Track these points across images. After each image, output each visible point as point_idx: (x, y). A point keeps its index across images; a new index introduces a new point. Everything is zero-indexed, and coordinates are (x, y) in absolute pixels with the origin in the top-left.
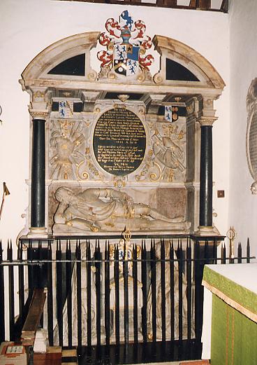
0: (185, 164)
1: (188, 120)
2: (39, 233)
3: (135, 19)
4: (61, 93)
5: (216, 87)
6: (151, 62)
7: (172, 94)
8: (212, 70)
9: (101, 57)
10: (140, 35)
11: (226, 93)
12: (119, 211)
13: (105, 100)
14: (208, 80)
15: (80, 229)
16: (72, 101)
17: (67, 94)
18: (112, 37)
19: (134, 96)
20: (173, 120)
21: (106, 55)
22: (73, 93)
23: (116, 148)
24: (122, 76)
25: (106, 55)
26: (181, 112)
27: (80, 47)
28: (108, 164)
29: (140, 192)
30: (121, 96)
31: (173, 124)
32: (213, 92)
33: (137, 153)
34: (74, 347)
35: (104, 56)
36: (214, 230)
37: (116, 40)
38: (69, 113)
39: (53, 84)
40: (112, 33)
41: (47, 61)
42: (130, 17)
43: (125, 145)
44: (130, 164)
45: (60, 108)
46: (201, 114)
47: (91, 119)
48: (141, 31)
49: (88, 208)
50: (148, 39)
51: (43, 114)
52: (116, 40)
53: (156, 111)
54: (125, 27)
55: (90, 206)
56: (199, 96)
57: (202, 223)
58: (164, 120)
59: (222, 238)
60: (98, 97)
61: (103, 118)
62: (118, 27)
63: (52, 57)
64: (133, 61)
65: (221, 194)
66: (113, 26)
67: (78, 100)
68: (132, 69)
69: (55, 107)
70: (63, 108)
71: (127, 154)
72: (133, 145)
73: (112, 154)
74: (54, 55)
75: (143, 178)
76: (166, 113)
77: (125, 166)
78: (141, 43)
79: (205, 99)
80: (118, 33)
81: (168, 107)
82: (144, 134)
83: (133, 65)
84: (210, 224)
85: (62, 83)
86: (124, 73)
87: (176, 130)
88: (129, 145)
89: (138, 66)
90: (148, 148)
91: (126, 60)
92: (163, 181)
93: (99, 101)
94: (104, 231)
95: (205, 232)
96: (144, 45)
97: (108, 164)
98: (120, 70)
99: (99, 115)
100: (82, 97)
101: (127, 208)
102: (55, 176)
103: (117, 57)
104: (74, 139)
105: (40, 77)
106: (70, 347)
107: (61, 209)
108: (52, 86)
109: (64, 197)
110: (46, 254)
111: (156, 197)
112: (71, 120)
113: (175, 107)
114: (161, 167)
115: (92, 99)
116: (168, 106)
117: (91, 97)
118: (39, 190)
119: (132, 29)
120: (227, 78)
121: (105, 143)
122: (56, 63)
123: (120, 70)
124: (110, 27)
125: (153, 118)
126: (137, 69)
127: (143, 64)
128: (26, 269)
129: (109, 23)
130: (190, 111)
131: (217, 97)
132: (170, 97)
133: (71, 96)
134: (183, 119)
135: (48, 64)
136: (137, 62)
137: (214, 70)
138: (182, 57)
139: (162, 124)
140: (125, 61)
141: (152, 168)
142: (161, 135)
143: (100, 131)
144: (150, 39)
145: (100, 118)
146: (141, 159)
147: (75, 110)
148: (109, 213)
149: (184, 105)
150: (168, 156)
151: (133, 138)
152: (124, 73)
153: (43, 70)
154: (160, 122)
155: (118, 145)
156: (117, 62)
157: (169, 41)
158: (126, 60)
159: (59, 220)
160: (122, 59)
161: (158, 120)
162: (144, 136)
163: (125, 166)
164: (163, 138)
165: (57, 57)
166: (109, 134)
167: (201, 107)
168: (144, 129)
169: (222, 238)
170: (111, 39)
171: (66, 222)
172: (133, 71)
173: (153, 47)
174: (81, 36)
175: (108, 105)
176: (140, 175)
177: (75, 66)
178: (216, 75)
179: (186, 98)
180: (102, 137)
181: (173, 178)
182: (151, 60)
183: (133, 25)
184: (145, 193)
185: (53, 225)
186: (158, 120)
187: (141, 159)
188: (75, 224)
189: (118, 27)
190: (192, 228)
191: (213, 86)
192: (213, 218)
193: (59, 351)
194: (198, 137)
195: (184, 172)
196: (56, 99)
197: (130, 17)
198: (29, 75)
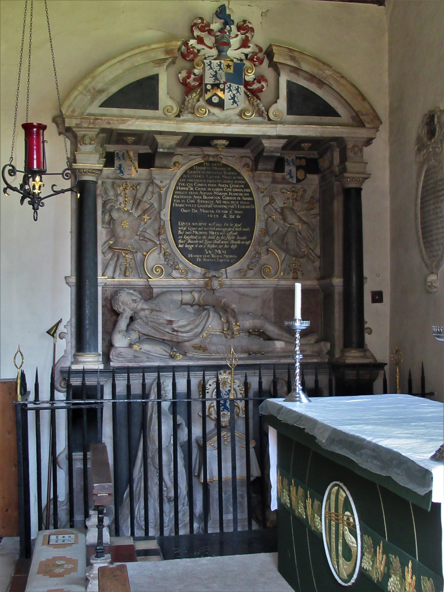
0: (318, 251)
1: (323, 179)
2: (91, 361)
3: (236, 17)
4: (119, 137)
5: (367, 125)
6: (263, 87)
7: (295, 137)
8: (360, 98)
9: (185, 80)
10: (245, 44)
11: (382, 138)
12: (214, 323)
13: (189, 149)
14: (354, 114)
15: (155, 355)
16: (134, 151)
17: (131, 139)
18: (199, 47)
19: (236, 142)
20: (298, 181)
21: (193, 76)
22: (140, 137)
23: (207, 226)
24: (216, 111)
25: (193, 76)
26: (311, 167)
27: (151, 64)
28: (196, 251)
29: (247, 296)
30: (216, 142)
31: (299, 186)
32: (363, 133)
33: (241, 234)
34: (153, 538)
35: (189, 77)
36: (368, 354)
37: (207, 52)
38: (135, 172)
39: (109, 123)
40: (200, 41)
41: (100, 86)
42: (229, 15)
43: (220, 219)
44: (230, 251)
45: (117, 163)
46: (344, 170)
47: (168, 179)
48: (247, 37)
49: (165, 322)
50: (257, 50)
51: (92, 171)
52: (207, 52)
53: (271, 165)
54: (222, 30)
55: (169, 318)
56: (340, 142)
57: (347, 345)
58: (284, 181)
59: (381, 366)
60: (180, 144)
61: (185, 177)
62: (210, 32)
63: (107, 80)
64: (234, 86)
65: (377, 297)
66: (202, 30)
67: (145, 149)
68: (233, 98)
69: (109, 160)
70: (122, 162)
71: (225, 235)
72: (235, 221)
73: (202, 235)
74: (111, 77)
75: (251, 273)
76: (287, 168)
77: (222, 254)
78: (246, 55)
79: (350, 145)
80: (209, 40)
81: (290, 159)
82: (253, 202)
83: (235, 92)
84: (361, 345)
85: (124, 122)
86: (221, 105)
87: (302, 196)
88: (228, 220)
89: (242, 93)
90: (258, 226)
91: (225, 83)
92: (283, 278)
93: (179, 150)
94: (191, 359)
95: (353, 357)
96: (251, 60)
97: (196, 251)
98: (215, 100)
99: (179, 172)
100: (154, 144)
101: (228, 322)
102: (110, 272)
103: (209, 80)
104: (140, 212)
105: (87, 112)
106: (147, 537)
107: (123, 324)
108: (108, 126)
109: (127, 303)
110: (94, 392)
111: (272, 304)
112: (134, 182)
113: (300, 158)
114: (280, 256)
115: (170, 148)
116: (290, 156)
117: (168, 145)
118: (354, 278)
119: (232, 35)
120: (383, 112)
121: (191, 218)
122: (114, 89)
123: (215, 100)
124: (197, 33)
125: (266, 177)
126: (241, 98)
127: (250, 90)
128: (62, 417)
129: (195, 25)
130: (324, 164)
131: (369, 142)
132: (293, 143)
133: (135, 143)
134: (314, 179)
135: (101, 91)
136: (242, 88)
137: (364, 99)
138: (312, 78)
139: (280, 186)
140: (222, 86)
141: (264, 258)
142: (279, 203)
143: (181, 199)
144: (261, 50)
145: (182, 177)
146: (247, 243)
147: (141, 166)
148: (199, 329)
149: (314, 155)
150: (290, 238)
151: (234, 209)
152: (221, 105)
153: (92, 101)
154: (278, 183)
155: (211, 220)
156: (209, 87)
157: (292, 53)
158: (225, 83)
159: (120, 341)
160: (218, 82)
161: (274, 181)
162: (252, 207)
163: (222, 254)
164: (282, 209)
165: (115, 80)
166: (196, 203)
167: (344, 159)
168: (251, 195)
169: (387, 364)
170: (199, 51)
171: (131, 346)
172: (235, 102)
173: (266, 62)
174: (153, 46)
175: (194, 158)
176: (246, 268)
177: (141, 93)
178: (368, 106)
179: (317, 143)
180: (185, 208)
181: (299, 273)
182: (263, 83)
183: (234, 27)
184: (256, 297)
185: (109, 346)
186: (274, 181)
187: (247, 243)
188: (146, 347)
189: (210, 32)
190: (331, 353)
191: (361, 125)
192: (366, 335)
193: (130, 542)
194: (338, 206)
195: (317, 264)
196: (111, 148)
197: (229, 15)
198: (71, 109)
